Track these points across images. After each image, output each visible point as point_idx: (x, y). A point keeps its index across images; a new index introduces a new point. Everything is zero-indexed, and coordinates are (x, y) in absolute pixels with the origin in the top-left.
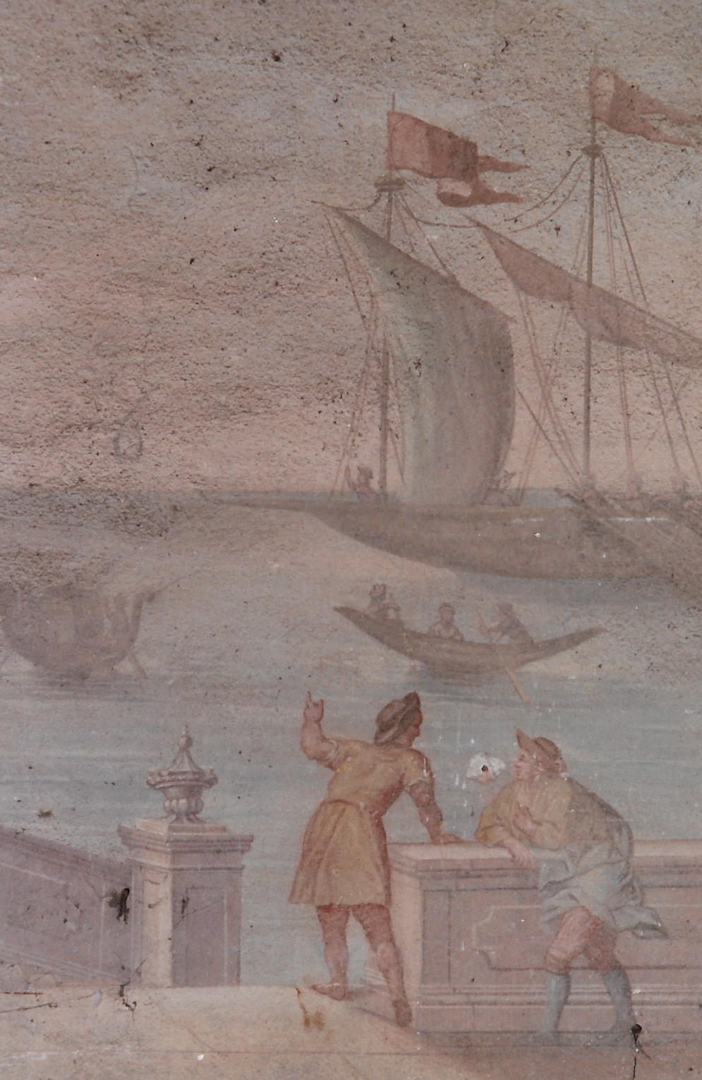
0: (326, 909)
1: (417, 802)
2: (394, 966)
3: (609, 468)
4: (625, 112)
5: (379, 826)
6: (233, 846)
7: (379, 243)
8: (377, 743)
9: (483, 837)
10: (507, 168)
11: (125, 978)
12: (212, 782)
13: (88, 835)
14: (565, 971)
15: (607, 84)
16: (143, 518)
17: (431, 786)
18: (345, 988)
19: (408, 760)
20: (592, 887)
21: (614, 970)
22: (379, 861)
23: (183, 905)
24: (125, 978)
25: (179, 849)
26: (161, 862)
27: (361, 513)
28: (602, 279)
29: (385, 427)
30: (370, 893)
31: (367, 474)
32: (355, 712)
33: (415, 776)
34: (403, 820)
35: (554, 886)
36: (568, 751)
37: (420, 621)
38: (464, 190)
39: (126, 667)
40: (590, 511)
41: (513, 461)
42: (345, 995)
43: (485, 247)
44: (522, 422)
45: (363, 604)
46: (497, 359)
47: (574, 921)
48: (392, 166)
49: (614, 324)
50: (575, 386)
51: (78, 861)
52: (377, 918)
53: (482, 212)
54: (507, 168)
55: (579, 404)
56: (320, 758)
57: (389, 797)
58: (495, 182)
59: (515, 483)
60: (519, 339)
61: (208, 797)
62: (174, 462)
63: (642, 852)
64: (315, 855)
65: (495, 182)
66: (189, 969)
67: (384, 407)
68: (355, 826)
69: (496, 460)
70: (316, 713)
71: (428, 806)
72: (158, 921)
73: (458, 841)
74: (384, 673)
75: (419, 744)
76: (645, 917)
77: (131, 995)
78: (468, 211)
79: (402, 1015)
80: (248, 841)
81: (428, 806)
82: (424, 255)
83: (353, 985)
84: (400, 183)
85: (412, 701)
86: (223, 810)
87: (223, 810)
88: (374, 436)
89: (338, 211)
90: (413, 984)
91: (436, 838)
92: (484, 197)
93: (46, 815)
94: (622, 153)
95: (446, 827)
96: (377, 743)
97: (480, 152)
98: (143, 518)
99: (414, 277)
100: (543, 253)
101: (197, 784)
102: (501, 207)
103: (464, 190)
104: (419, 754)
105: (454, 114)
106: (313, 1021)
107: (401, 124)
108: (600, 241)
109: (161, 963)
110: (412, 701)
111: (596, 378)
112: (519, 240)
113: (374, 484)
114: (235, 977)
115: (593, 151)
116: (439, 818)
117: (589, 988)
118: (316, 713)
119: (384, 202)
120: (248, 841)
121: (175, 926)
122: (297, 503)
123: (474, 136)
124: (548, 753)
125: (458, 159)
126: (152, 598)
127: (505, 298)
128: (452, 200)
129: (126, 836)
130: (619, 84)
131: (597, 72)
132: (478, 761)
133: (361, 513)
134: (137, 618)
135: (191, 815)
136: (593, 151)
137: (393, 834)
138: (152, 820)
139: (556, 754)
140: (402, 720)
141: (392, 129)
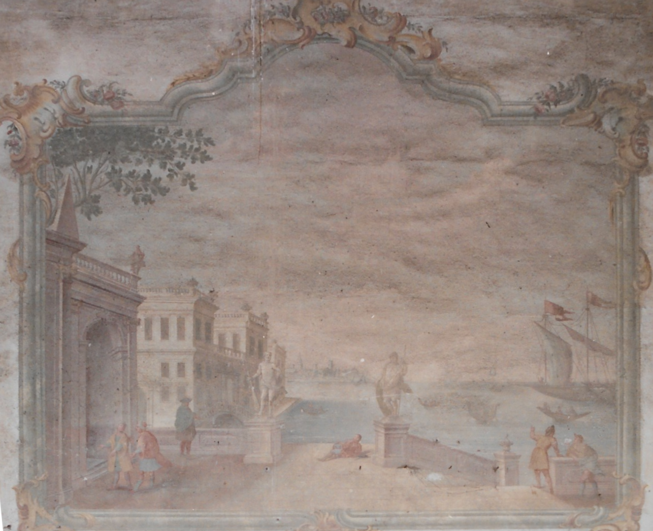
0: (536, 470)
1: (554, 448)
2: (550, 481)
3: (592, 377)
4: (594, 301)
5: (546, 453)
6: (516, 457)
7: (544, 329)
8: (546, 436)
9: (568, 455)
10: (569, 313)
11: (496, 484)
12: (512, 444)
13: (488, 455)
14: (584, 482)
15: (590, 295)
16: (497, 388)
17: (557, 444)
18: (121, 358)
19: (552, 440)
20: (590, 466)
21: (595, 483)
22: (108, 293)
23: (507, 470)
24: (496, 484)
25: (506, 458)
26: (502, 461)
27: (541, 387)
28: (590, 336)
29: (546, 369)
30: (545, 467)
31: (542, 379)
32: (541, 429)
33: (554, 443)
34: (551, 452)
35: (582, 465)
36: (585, 438)
37: (554, 410)
38: (561, 317)
39: (494, 420)
40: (588, 386)
41: (573, 376)
42: (540, 487)
43: (566, 330)
44: (574, 369)
45: (542, 406)
46: (569, 354)
47: (586, 472)
48: (546, 312)
49: (593, 346)
50: (585, 359)
51: (485, 460)
52: (546, 472)
53: (565, 323)
54: (569, 313)
55: (586, 364)
56: (534, 439)
57: (548, 447)
58: (567, 316)
59: (573, 381)
60: (573, 349)
61: (512, 447)
62: (502, 376)
63: (601, 458)
64: (534, 459)
65: (567, 316)
66: (510, 482)
67: (546, 364)
68: (542, 453)
69: (569, 376)
70: (533, 430)
71: (556, 449)
72: (502, 472)
73: (562, 456)
74: (547, 421)
75: (554, 436)
76: (600, 472)
77: (498, 487)
78: (562, 322)
79: (552, 492)
80: (520, 456)
81: (556, 449)
82: (553, 331)
83: (542, 486)
84: (547, 316)
85: (553, 427)
86: (515, 449)
87: (515, 449)
88: (544, 370)
89: (535, 322)
90: (554, 485)
91: (558, 456)
92: (566, 319)
93: (479, 451)
94: (594, 310)
95: (560, 453)
96: (546, 436)
97: (564, 310)
98: (497, 388)
99: (551, 336)
100: (578, 331)
101: (509, 444)
102: (568, 321)
103: (561, 317)
104: (555, 438)
105: (559, 301)
106: (534, 493)
107: (547, 303)
108: (590, 329)
109: (503, 480)
110: (553, 427)
111: (590, 358)
112: (573, 328)
113: (544, 381)
114: (518, 484)
115: (588, 309)
116: (559, 452)
117: (590, 486)
118: (533, 430)
119: (544, 320)
120: (520, 456)
121: (506, 474)
122: (526, 385)
123: (563, 306)
124: (581, 438)
125: (559, 311)
126: (499, 405)
127: (570, 340)
128: (558, 320)
129: (495, 455)
130: (593, 295)
131: (588, 292)
132: (566, 440)
133: (541, 387)
134: (496, 409)
135: (508, 451)
136: (588, 309)
137: (549, 454)
138: (501, 452)
139: (582, 438)
140: (551, 431)
141: (545, 304)
